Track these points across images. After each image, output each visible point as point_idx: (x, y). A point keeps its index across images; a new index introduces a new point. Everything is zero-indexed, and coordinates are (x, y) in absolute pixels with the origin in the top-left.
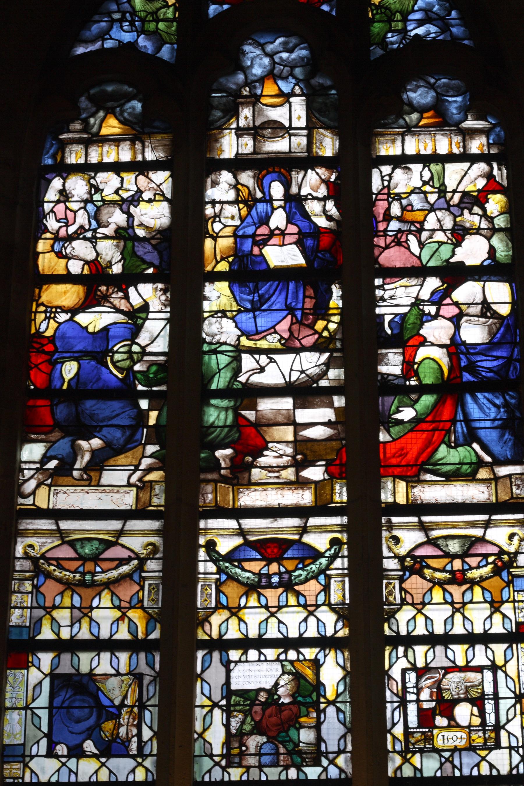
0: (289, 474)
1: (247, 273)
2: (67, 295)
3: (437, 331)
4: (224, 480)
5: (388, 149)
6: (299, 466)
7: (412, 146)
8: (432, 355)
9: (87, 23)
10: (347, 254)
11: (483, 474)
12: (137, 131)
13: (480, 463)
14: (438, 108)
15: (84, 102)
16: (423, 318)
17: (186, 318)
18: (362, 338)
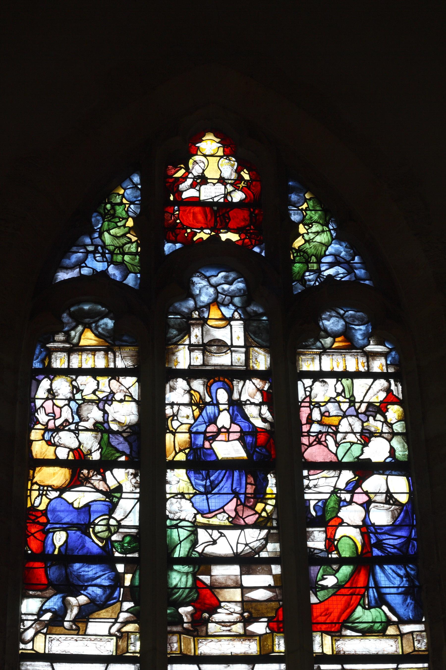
0: (238, 628)
1: (200, 462)
2: (57, 476)
3: (352, 514)
4: (187, 632)
5: (308, 365)
6: (246, 622)
7: (328, 363)
8: (349, 536)
9: (67, 253)
10: (278, 451)
11: (391, 630)
12: (111, 343)
13: (389, 622)
14: (347, 334)
15: (66, 318)
16: (340, 504)
17: (153, 498)
18: (293, 519)
